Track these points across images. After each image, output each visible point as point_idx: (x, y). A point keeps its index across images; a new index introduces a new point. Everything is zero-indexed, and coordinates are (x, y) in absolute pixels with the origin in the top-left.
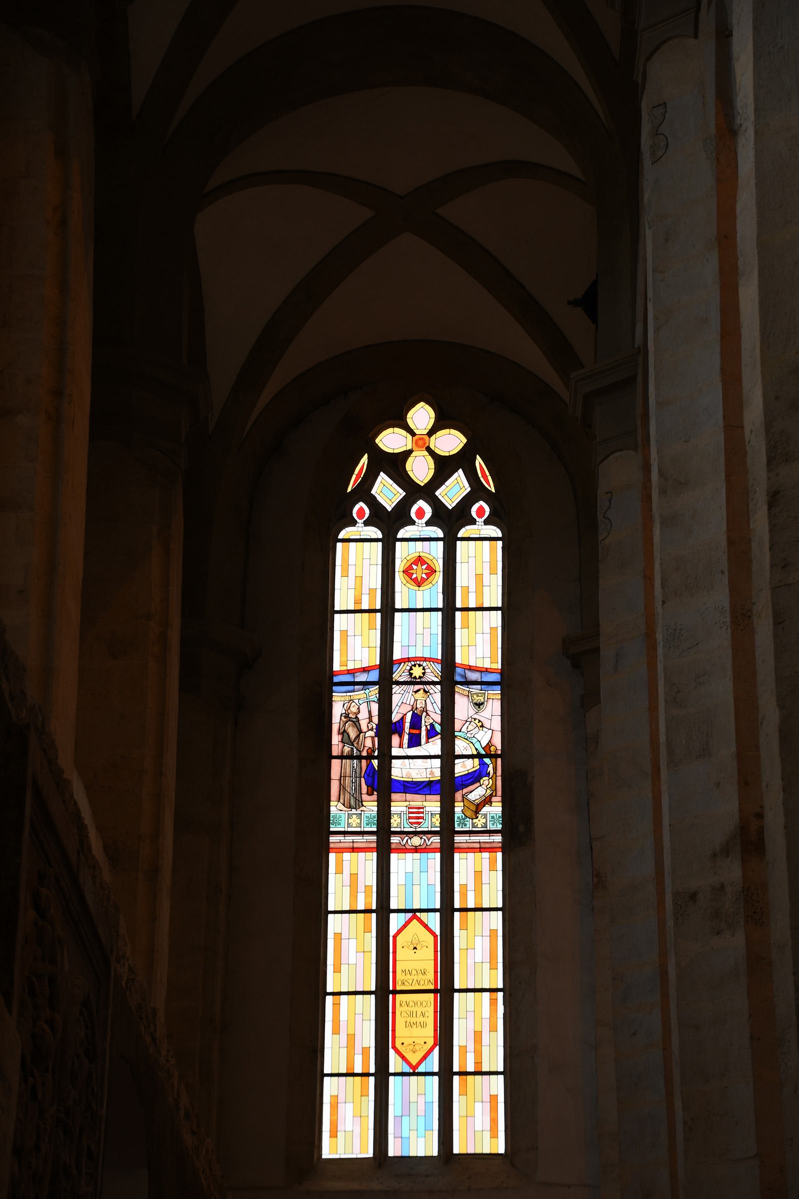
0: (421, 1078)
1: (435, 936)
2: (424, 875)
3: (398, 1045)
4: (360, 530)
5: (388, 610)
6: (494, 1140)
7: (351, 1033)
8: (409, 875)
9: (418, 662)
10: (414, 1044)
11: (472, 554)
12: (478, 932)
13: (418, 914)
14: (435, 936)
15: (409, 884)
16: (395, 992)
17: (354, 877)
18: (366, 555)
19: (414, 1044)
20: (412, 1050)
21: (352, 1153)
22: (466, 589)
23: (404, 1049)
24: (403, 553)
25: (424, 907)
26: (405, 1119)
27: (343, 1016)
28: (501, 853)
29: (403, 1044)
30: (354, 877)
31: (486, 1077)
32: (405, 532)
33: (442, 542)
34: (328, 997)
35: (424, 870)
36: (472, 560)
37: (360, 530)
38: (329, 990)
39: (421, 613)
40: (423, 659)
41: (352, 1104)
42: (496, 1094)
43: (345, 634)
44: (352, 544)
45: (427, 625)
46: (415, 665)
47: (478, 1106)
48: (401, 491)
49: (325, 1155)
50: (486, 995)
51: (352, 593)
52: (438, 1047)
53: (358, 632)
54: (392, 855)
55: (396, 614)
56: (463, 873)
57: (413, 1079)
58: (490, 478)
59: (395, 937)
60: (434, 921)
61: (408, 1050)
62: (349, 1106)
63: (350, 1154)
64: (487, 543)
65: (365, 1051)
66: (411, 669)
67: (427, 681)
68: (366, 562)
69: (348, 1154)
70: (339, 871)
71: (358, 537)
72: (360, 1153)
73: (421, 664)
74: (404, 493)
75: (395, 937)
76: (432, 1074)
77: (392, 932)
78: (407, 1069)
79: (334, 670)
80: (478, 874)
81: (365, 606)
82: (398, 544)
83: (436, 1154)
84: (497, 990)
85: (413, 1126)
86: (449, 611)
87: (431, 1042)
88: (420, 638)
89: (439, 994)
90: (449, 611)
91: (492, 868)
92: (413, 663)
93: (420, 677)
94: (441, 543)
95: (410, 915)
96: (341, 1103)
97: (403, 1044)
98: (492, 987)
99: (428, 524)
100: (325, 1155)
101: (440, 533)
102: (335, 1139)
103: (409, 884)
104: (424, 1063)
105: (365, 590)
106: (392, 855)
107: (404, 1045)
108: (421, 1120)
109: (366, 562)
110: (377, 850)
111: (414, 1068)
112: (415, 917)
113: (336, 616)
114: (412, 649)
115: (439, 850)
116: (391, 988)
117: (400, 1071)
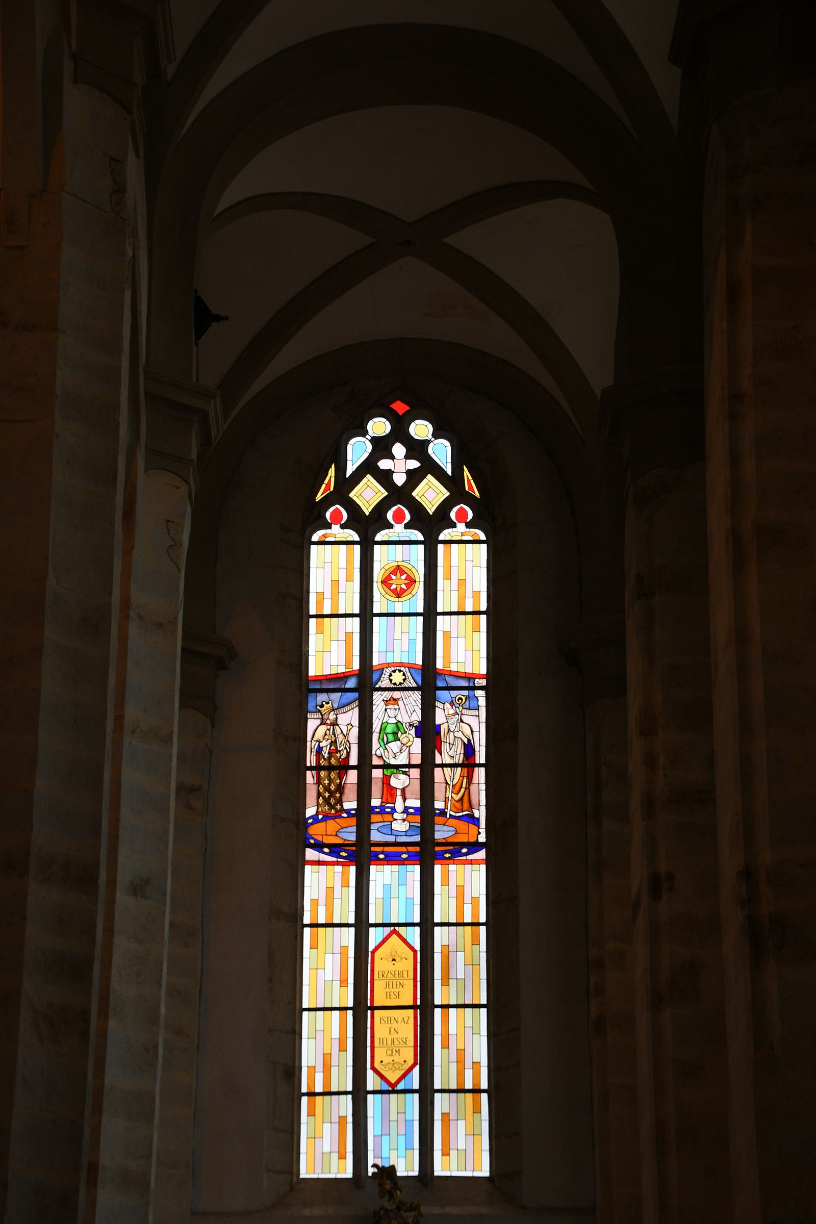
0: (401, 1096)
1: (415, 952)
2: (402, 888)
3: (377, 1065)
4: (336, 532)
5: (366, 615)
6: (342, 1161)
7: (327, 1052)
8: (387, 888)
9: (398, 668)
10: (393, 1062)
11: (328, 559)
12: (329, 950)
13: (397, 928)
14: (415, 952)
15: (386, 900)
16: (373, 1008)
17: (460, 890)
18: (469, 557)
19: (393, 1062)
20: (391, 1069)
21: (314, 1173)
22: (320, 595)
23: (383, 1067)
24: (383, 558)
25: (403, 921)
26: (385, 1139)
27: (452, 1030)
28: (485, 866)
29: (382, 1062)
30: (460, 890)
31: (335, 1097)
32: (445, 535)
33: (423, 546)
34: (436, 1010)
35: (402, 882)
36: (328, 566)
37: (336, 532)
38: (305, 1005)
39: (400, 618)
40: (401, 665)
41: (464, 1121)
42: (345, 1115)
43: (447, 635)
44: (454, 546)
45: (405, 630)
46: (394, 671)
47: (327, 1127)
48: (383, 490)
49: (401, 1171)
50: (336, 1013)
51: (455, 595)
52: (418, 1066)
53: (462, 634)
54: (306, 866)
55: (438, 617)
56: (315, 886)
57: (393, 1097)
58: (326, 482)
59: (373, 952)
60: (414, 935)
61: (387, 1069)
62: (461, 1124)
63: (343, 1173)
64: (343, 547)
65: (476, 1065)
66: (391, 675)
67: (407, 686)
68: (469, 564)
69: (342, 1173)
70: (445, 882)
71: (397, 539)
72: (322, 1173)
73: (402, 670)
74: (387, 493)
75: (373, 952)
76: (412, 1091)
77: (371, 947)
78: (386, 1087)
79: (309, 675)
80: (330, 890)
81: (469, 608)
82: (376, 547)
83: (484, 1171)
84: (346, 1009)
85: (394, 1146)
86: (430, 614)
87: (411, 1061)
88: (397, 643)
89: (418, 1010)
90: (430, 614)
91: (345, 884)
92: (393, 669)
93: (401, 684)
94: (421, 547)
95: (388, 930)
96: (336, 1123)
97: (382, 1062)
98: (443, 1003)
99: (407, 526)
100: (401, 1171)
101: (354, 536)
102: (448, 1157)
103: (386, 900)
104: (403, 1082)
105: (469, 593)
106: (371, 866)
107: (383, 1063)
108: (402, 1139)
109: (469, 564)
110: (420, 862)
111: (393, 1085)
112: (394, 932)
113: (439, 618)
114: (390, 655)
115: (484, 862)
116: (369, 1005)
117: (379, 1089)
